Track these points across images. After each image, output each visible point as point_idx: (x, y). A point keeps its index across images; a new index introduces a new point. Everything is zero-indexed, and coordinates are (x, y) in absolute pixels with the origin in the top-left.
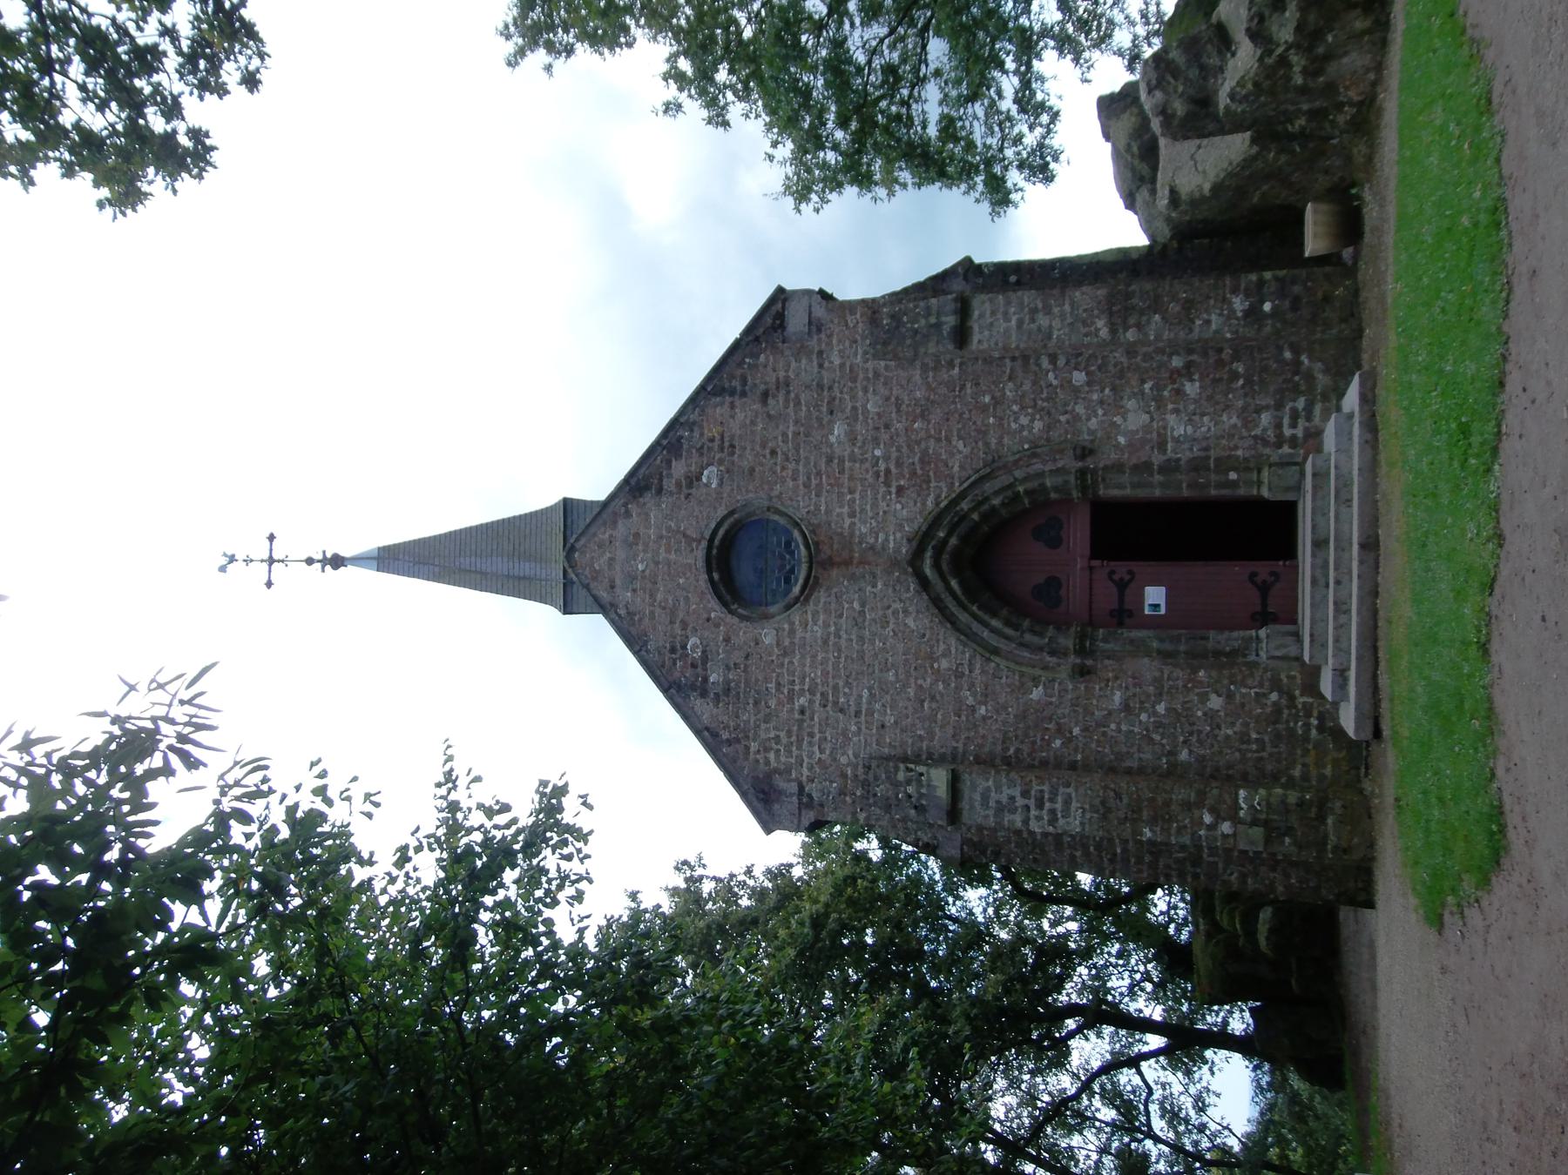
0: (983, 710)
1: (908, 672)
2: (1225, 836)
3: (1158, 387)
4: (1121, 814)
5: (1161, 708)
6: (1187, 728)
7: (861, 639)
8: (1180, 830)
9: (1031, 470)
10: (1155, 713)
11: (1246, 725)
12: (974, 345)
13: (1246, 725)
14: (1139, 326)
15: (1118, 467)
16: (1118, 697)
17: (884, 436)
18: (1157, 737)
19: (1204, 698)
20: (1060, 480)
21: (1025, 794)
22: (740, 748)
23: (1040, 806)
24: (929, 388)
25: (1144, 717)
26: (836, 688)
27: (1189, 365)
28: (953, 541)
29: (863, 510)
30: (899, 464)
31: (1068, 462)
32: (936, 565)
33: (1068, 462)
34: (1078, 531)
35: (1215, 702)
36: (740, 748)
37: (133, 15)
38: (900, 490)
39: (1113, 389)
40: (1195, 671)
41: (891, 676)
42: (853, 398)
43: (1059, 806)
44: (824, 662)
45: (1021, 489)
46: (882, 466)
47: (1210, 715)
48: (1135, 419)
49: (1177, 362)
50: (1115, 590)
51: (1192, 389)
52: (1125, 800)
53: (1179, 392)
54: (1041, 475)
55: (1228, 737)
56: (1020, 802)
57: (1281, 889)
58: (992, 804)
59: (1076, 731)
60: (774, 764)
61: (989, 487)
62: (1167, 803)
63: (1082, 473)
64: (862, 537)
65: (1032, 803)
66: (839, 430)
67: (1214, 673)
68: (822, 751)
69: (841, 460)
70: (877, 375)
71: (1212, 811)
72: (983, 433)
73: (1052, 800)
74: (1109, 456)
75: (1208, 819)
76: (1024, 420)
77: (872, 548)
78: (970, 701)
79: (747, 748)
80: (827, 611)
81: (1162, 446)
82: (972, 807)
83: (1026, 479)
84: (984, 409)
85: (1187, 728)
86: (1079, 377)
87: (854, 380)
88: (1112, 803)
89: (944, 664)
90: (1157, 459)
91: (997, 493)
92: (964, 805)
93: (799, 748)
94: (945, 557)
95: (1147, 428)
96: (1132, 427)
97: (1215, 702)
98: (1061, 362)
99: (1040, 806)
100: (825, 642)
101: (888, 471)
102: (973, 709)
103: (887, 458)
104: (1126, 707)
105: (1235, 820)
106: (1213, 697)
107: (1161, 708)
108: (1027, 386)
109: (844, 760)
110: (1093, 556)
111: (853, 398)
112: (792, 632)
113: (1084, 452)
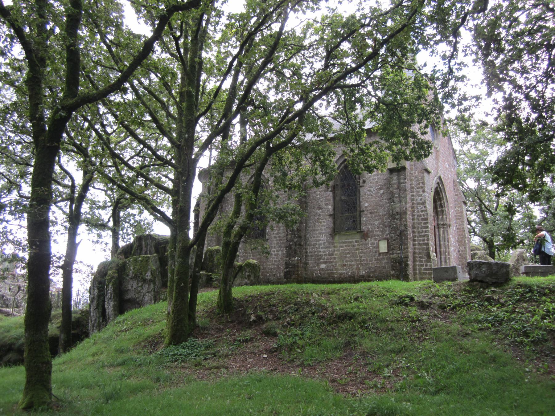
33: (448, 223)
113: (450, 226)
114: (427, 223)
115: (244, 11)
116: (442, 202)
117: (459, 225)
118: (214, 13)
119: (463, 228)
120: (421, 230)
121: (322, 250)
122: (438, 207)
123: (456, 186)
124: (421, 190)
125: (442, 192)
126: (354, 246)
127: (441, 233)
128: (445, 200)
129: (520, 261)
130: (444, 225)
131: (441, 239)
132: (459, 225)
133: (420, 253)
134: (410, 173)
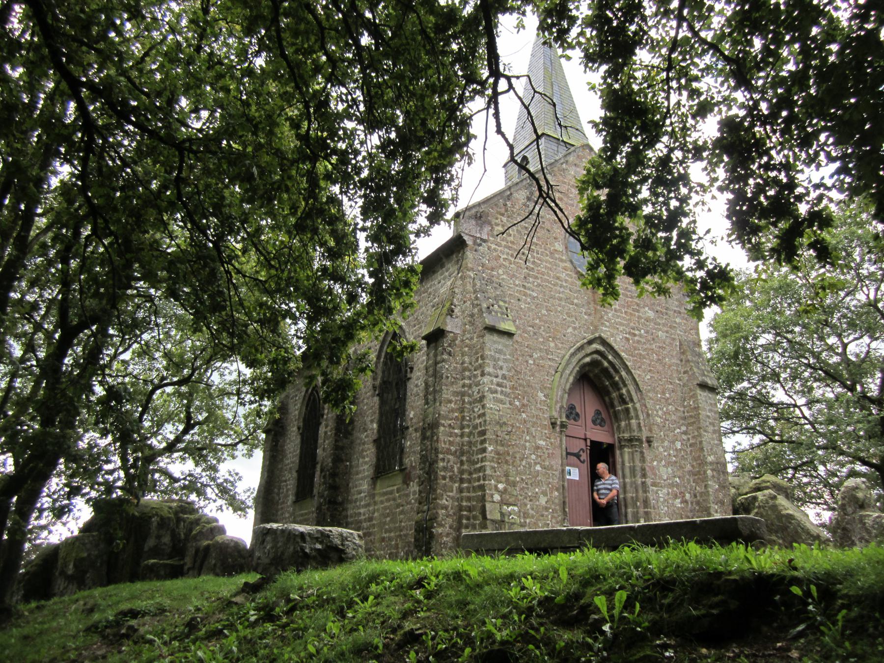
0: (531, 362)
1: (546, 322)
2: (492, 496)
3: (677, 486)
4: (499, 433)
5: (538, 468)
6: (530, 482)
7: (560, 299)
8: (493, 468)
9: (640, 413)
10: (536, 464)
11: (533, 517)
12: (699, 391)
13: (533, 517)
14: (713, 476)
15: (643, 459)
16: (542, 443)
17: (649, 338)
18: (524, 463)
19: (544, 493)
20: (635, 427)
21: (504, 377)
22: (503, 210)
23: (498, 385)
24: (670, 366)
25: (533, 457)
26: (536, 278)
27: (686, 502)
28: (606, 364)
29: (618, 317)
30: (638, 342)
31: (645, 434)
32: (597, 352)
33: (645, 434)
34: (601, 436)
35: (543, 500)
36: (503, 210)
37: (446, 187)
38: (627, 339)
39: (676, 462)
40: (557, 490)
41: (544, 312)
42: (664, 325)
43: (499, 396)
44: (549, 275)
45: (630, 406)
46: (637, 332)
47: (536, 497)
48: (665, 472)
49: (688, 496)
50: (576, 451)
51: (678, 502)
52: (507, 437)
53: (676, 497)
54: (637, 417)
55: (526, 505)
56: (500, 373)
57: (440, 530)
58: (497, 355)
59: (524, 415)
60: (496, 228)
61: (632, 388)
62: (507, 462)
63: (639, 440)
64: (607, 313)
65: (499, 380)
66: (651, 314)
67: (557, 501)
68: (505, 259)
69: (638, 311)
70: (674, 339)
71: (505, 489)
72: (654, 390)
73: (502, 392)
74: (648, 455)
75: (501, 486)
76: (660, 413)
77: (602, 317)
78: (535, 356)
79: (503, 215)
80: (572, 284)
81: (654, 484)
82: (495, 342)
83: (635, 409)
84: (663, 393)
85: (530, 482)
86: (678, 445)
87: (671, 327)
88: (505, 428)
89: (552, 345)
90: (649, 481)
91: (628, 391)
92: (495, 337)
93: (506, 247)
94: (599, 358)
95: (661, 477)
96: (661, 469)
97: (543, 500)
98: (685, 437)
99: (498, 385)
100: (558, 278)
101: (635, 335)
102: (531, 356)
103: (640, 336)
104: (538, 448)
105: (502, 502)
106: (545, 499)
107: (538, 468)
108: (674, 417)
109: (501, 272)
110: (592, 442)
111: (664, 325)
112: (562, 261)
113: (649, 441)
114: (485, 440)
115: (719, 135)
116: (624, 391)
117: (693, 437)
118: (187, 145)
119: (701, 442)
120: (475, 458)
121: (362, 511)
122: (616, 403)
123: (683, 353)
124: (478, 372)
125: (617, 371)
126: (394, 499)
127: (626, 457)
128: (632, 388)
129: (850, 510)
130: (630, 440)
131: (627, 471)
132: (693, 437)
133: (470, 509)
134: (462, 341)
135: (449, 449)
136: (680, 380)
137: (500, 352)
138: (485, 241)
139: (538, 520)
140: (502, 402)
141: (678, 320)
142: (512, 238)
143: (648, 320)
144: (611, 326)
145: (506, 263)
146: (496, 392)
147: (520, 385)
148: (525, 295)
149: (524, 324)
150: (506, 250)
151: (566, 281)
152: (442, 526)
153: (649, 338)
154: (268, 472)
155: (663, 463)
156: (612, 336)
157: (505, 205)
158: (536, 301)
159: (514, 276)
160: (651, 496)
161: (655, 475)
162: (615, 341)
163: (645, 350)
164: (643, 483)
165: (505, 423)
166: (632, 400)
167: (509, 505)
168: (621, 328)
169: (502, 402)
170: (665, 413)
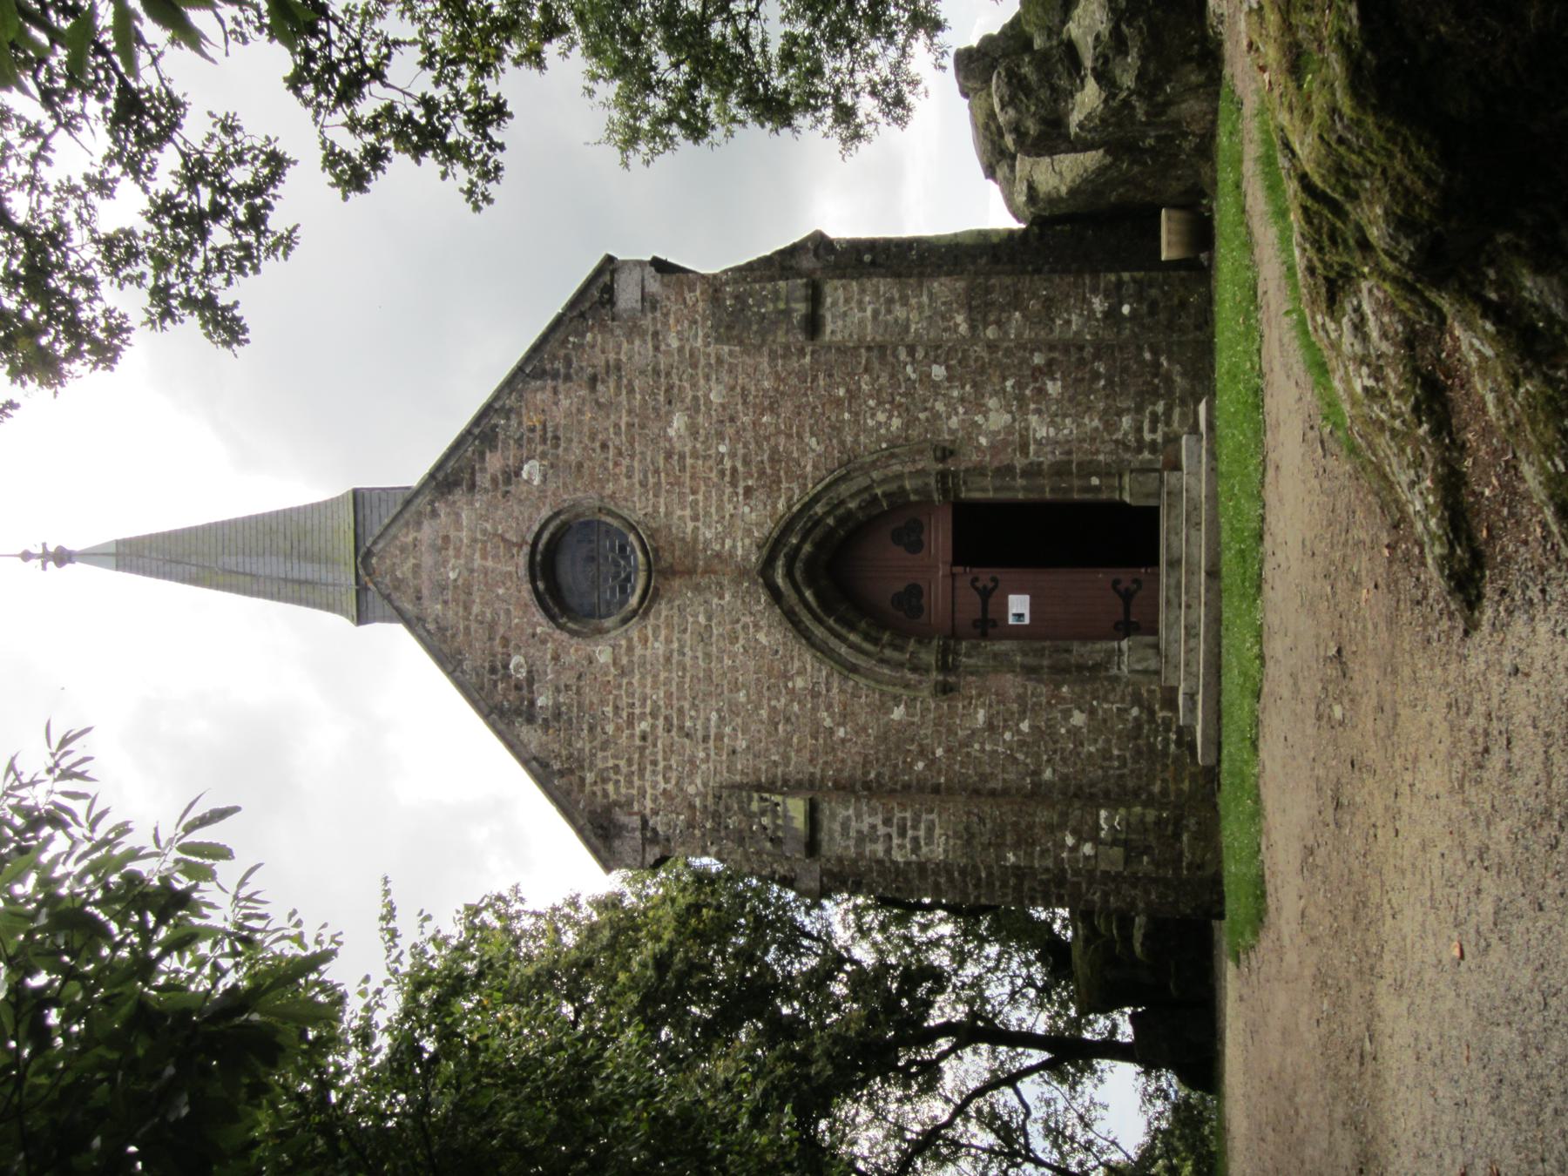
0: (841, 733)
2: (1087, 858)
3: (1020, 385)
4: (985, 840)
7: (708, 656)
10: (1019, 732)
11: (1108, 741)
16: (981, 715)
18: (1020, 756)
19: (1067, 714)
23: (902, 834)
24: (778, 377)
25: (1008, 736)
27: (1050, 363)
28: (807, 548)
29: (707, 514)
31: (927, 463)
38: (748, 491)
39: (974, 385)
40: (1058, 686)
41: (742, 696)
43: (922, 833)
44: (668, 682)
45: (879, 491)
47: (1074, 732)
50: (978, 599)
51: (1053, 388)
53: (1041, 391)
54: (900, 476)
56: (882, 830)
58: (853, 834)
59: (939, 752)
60: (613, 796)
61: (844, 490)
62: (1031, 827)
63: (943, 476)
65: (894, 831)
68: (667, 780)
71: (1074, 832)
77: (718, 555)
82: (832, 839)
87: (694, 366)
88: (975, 828)
90: (1019, 462)
92: (824, 836)
93: (642, 777)
94: (799, 565)
95: (1009, 429)
97: (1078, 718)
99: (902, 834)
104: (990, 726)
105: (1097, 841)
106: (1076, 713)
107: (1025, 726)
108: (884, 380)
109: (691, 790)
111: (694, 386)
113: (945, 453)
135: (1014, 889)
136: (802, 353)
137: (845, 826)
138: (645, 822)
139: (1111, 731)
140: (930, 829)
141: (675, 344)
142: (622, 763)
143: (693, 431)
144: (729, 531)
145: (674, 776)
146: (915, 840)
147: (887, 757)
148: (719, 737)
149: (777, 743)
150: (648, 774)
151: (668, 641)
152: (1134, 899)
153: (730, 430)
154: (974, 247)
155: (979, 419)
156: (748, 532)
157: (561, 773)
158: (725, 713)
159: (692, 761)
160: (1047, 459)
161: (1005, 443)
162: (760, 525)
163: (759, 446)
164: (1025, 473)
165: (967, 829)
166: (868, 488)
167: (1098, 828)
168: (729, 508)
169: (930, 829)
170: (880, 403)
